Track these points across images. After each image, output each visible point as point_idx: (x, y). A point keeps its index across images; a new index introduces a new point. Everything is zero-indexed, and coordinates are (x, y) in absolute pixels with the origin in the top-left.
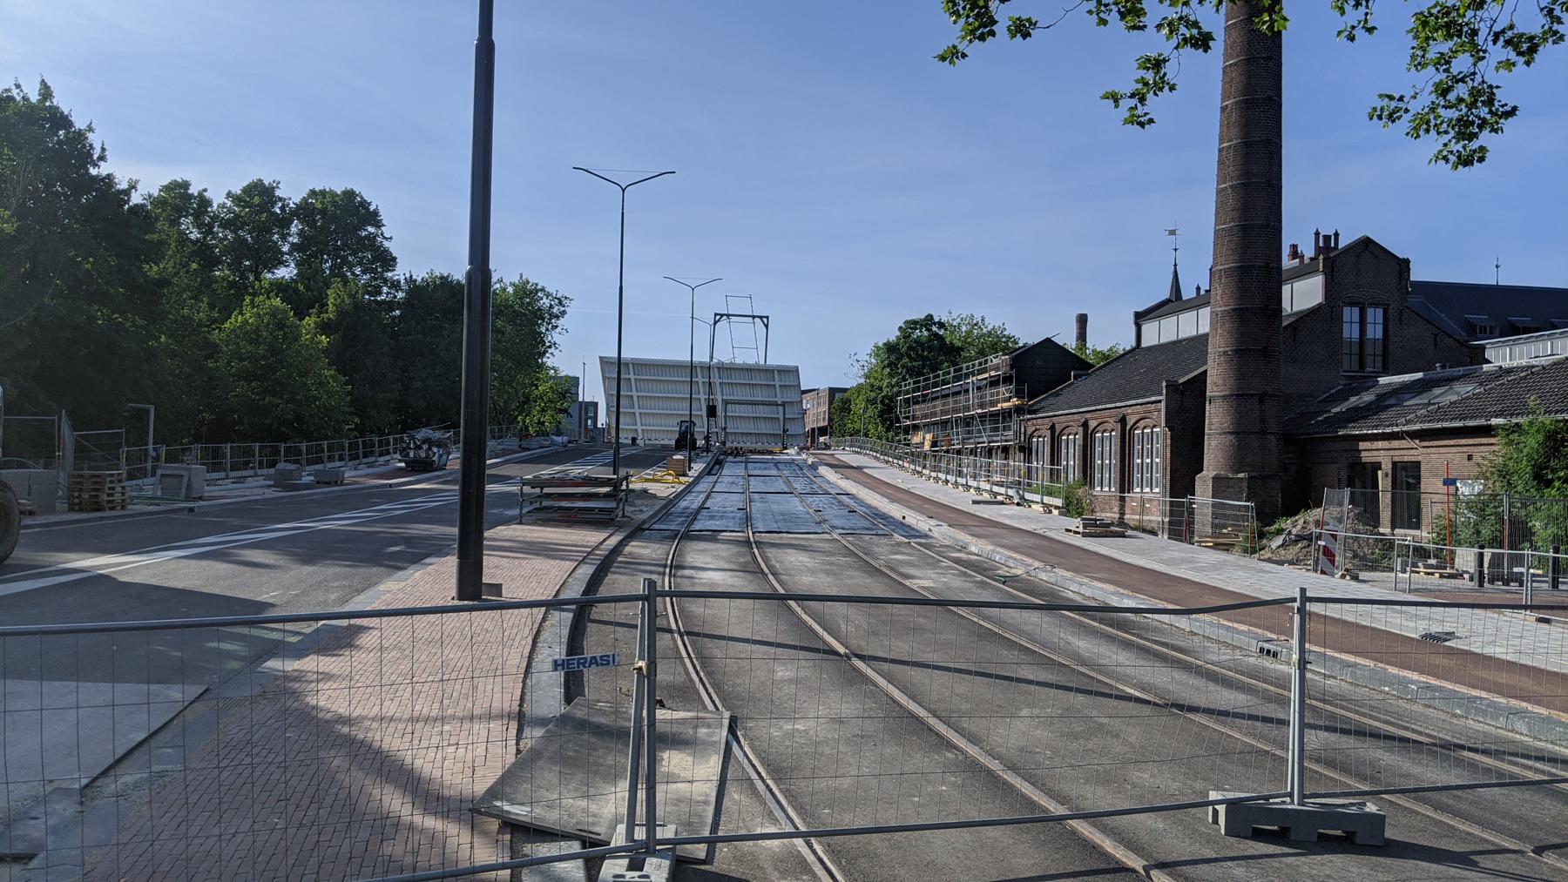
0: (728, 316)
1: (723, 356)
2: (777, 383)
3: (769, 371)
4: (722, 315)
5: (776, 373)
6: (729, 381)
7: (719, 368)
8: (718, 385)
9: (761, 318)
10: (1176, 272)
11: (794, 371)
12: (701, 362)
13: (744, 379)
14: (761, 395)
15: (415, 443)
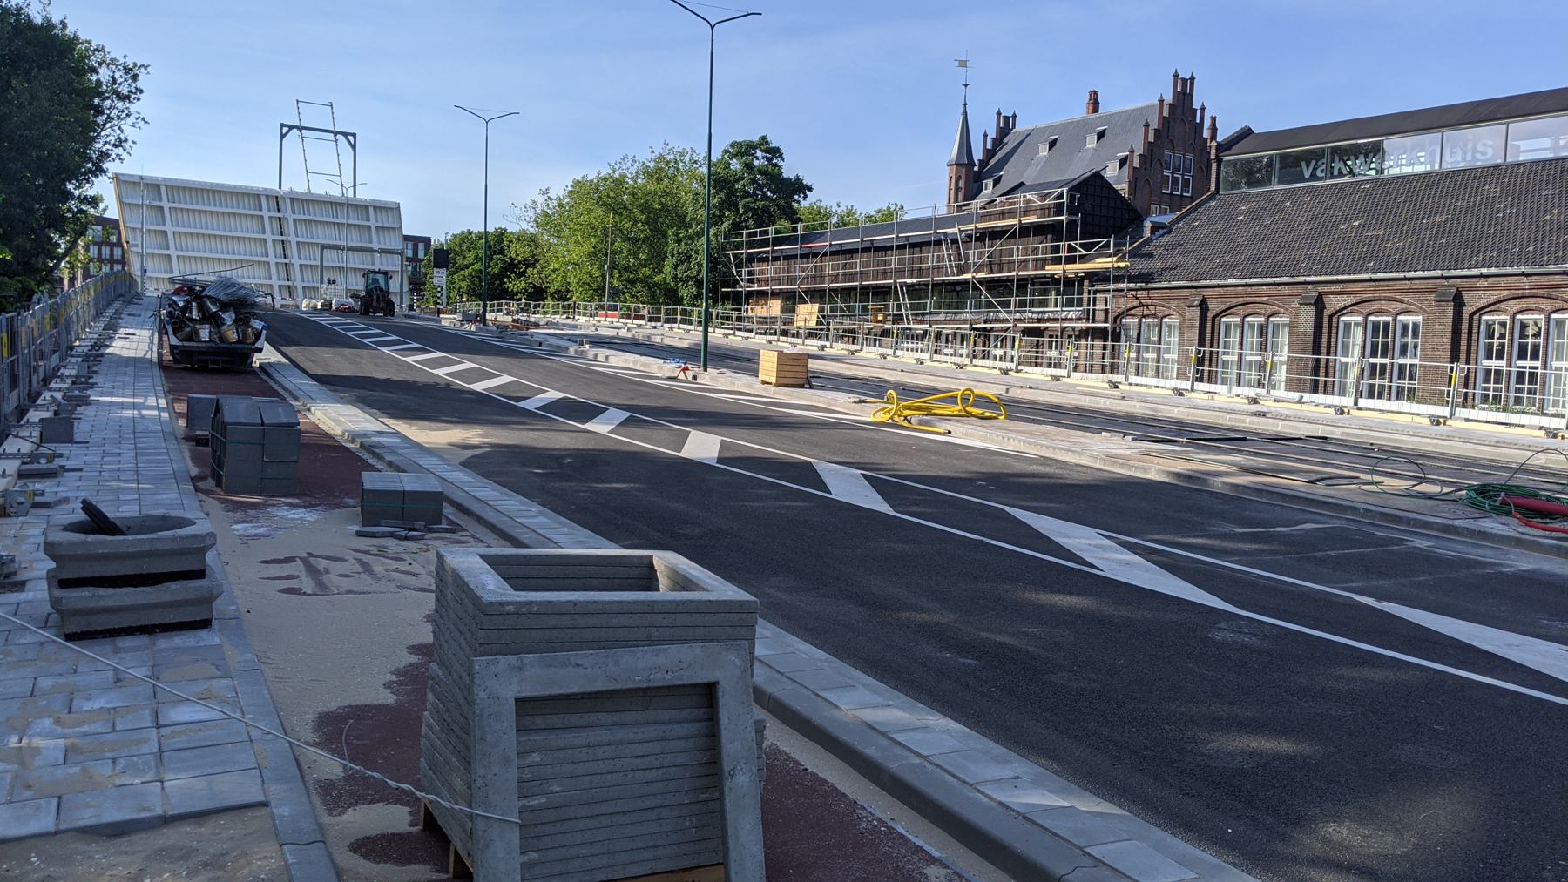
0: (300, 129)
1: (295, 183)
2: (373, 223)
3: (363, 208)
4: (291, 127)
5: (371, 210)
6: (306, 217)
7: (292, 199)
8: (291, 222)
9: (345, 135)
10: (965, 113)
11: (395, 209)
12: (266, 189)
13: (327, 216)
14: (354, 240)
15: (201, 308)
